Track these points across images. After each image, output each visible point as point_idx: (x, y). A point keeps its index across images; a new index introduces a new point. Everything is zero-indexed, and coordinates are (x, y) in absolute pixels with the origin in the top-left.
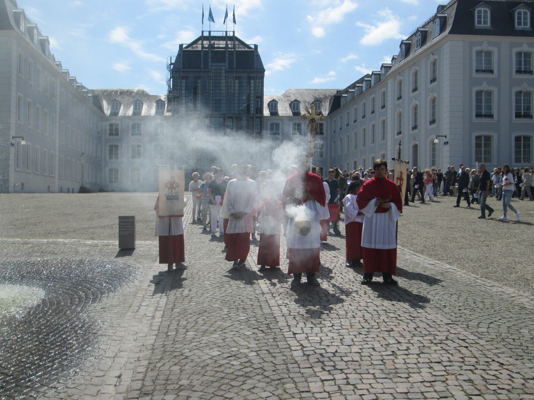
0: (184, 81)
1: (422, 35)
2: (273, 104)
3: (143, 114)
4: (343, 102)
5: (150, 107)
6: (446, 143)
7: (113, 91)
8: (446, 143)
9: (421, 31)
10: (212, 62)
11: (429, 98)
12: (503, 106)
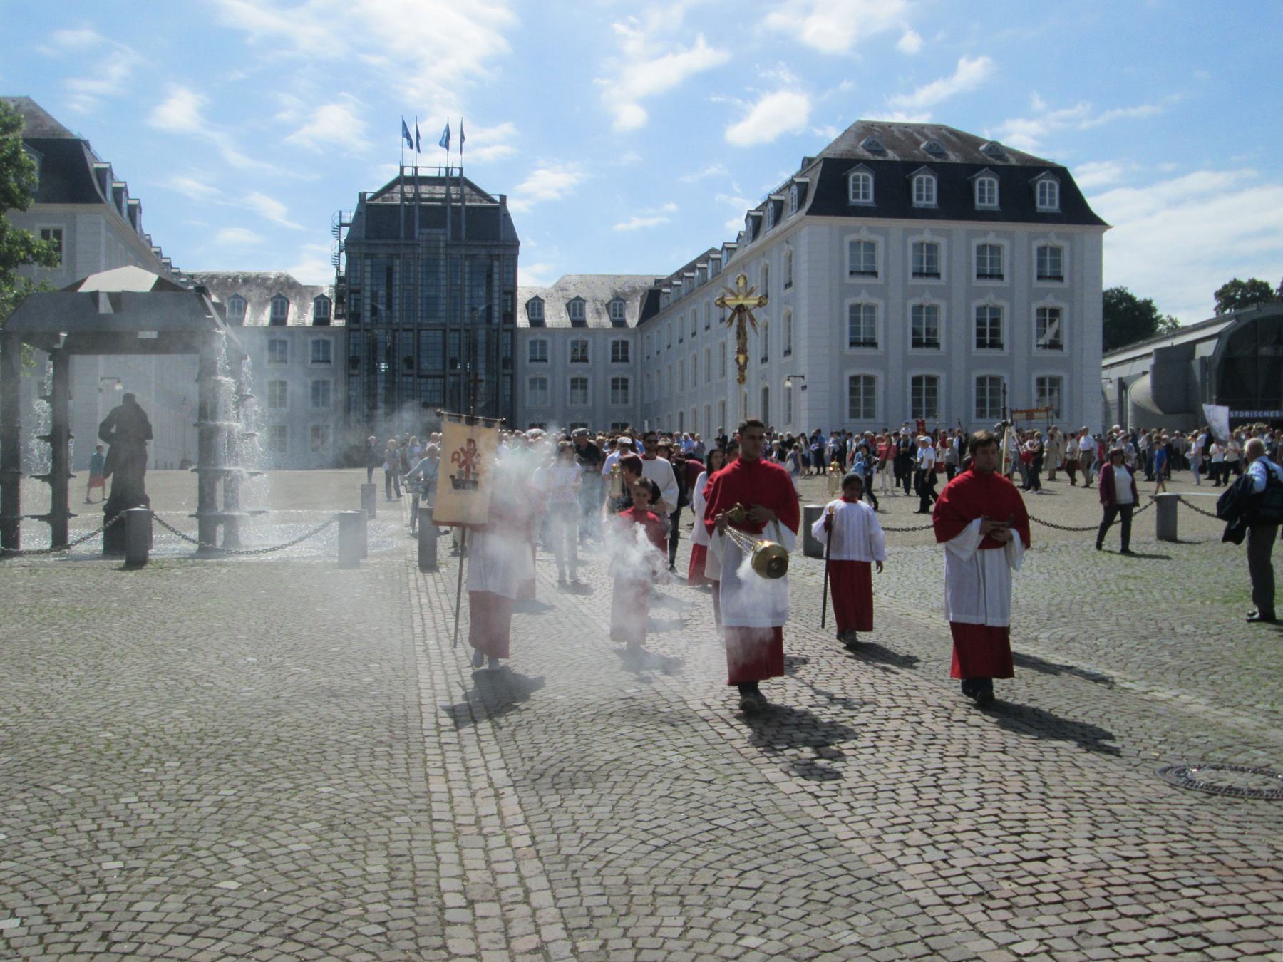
0: (368, 262)
1: (776, 208)
2: (535, 306)
3: (289, 323)
4: (663, 302)
5: (302, 309)
6: (804, 387)
7: (229, 277)
8: (804, 387)
9: (775, 201)
10: (421, 227)
11: (783, 313)
12: (892, 329)
